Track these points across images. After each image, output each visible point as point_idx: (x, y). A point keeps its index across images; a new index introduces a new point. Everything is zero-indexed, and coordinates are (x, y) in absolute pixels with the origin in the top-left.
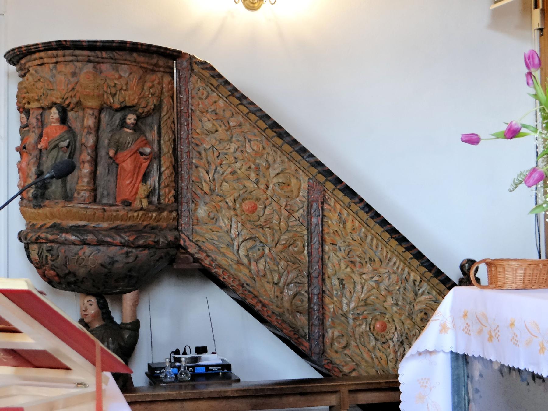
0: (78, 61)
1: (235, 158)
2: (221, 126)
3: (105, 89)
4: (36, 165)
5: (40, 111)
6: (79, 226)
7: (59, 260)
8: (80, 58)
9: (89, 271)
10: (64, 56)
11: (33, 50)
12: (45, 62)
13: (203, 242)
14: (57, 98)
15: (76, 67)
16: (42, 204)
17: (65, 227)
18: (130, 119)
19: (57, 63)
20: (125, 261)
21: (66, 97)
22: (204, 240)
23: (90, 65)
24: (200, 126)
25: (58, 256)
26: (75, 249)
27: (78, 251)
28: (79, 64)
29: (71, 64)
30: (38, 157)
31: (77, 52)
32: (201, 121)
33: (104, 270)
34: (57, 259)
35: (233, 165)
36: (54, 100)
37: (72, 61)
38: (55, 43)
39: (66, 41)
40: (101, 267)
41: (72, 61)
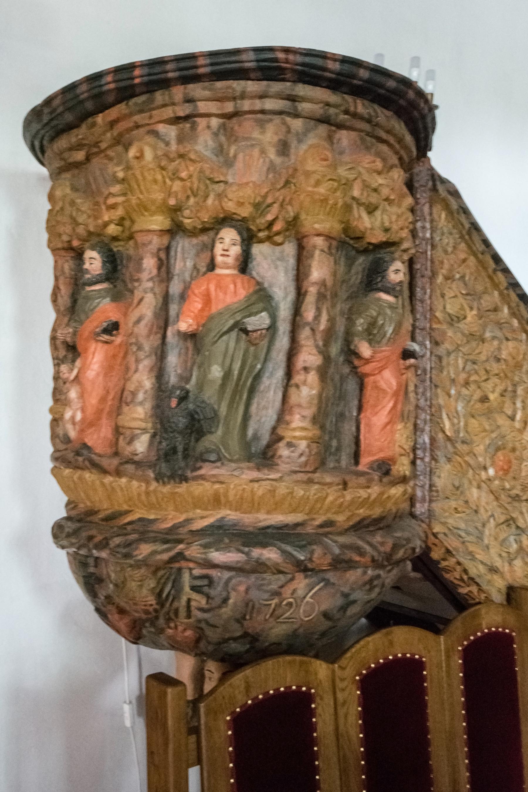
0: (296, 115)
1: (487, 371)
2: (471, 309)
3: (356, 193)
4: (154, 374)
5: (165, 240)
6: (286, 526)
7: (226, 611)
8: (305, 107)
9: (296, 630)
10: (262, 97)
11: (171, 75)
12: (202, 111)
13: (445, 534)
14: (241, 204)
15: (289, 131)
16: (189, 474)
17: (251, 529)
18: (397, 271)
19: (236, 114)
20: (367, 597)
21: (269, 200)
22: (446, 531)
23: (323, 129)
24: (441, 308)
25: (225, 600)
26: (274, 582)
27: (282, 587)
28: (297, 124)
29: (277, 119)
30: (159, 353)
31: (302, 90)
32: (443, 296)
33: (326, 624)
34: (220, 607)
35: (483, 384)
36: (230, 206)
37: (280, 113)
38: (252, 56)
39: (287, 50)
40: (323, 619)
41: (280, 113)
